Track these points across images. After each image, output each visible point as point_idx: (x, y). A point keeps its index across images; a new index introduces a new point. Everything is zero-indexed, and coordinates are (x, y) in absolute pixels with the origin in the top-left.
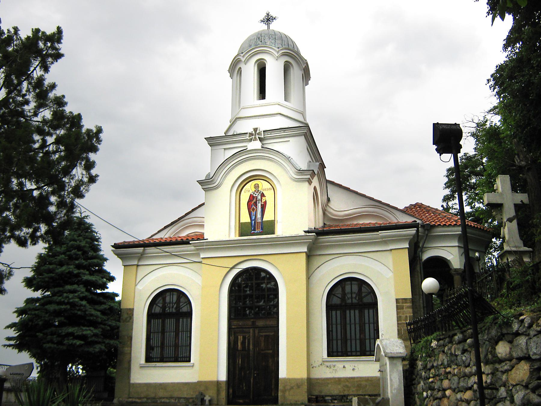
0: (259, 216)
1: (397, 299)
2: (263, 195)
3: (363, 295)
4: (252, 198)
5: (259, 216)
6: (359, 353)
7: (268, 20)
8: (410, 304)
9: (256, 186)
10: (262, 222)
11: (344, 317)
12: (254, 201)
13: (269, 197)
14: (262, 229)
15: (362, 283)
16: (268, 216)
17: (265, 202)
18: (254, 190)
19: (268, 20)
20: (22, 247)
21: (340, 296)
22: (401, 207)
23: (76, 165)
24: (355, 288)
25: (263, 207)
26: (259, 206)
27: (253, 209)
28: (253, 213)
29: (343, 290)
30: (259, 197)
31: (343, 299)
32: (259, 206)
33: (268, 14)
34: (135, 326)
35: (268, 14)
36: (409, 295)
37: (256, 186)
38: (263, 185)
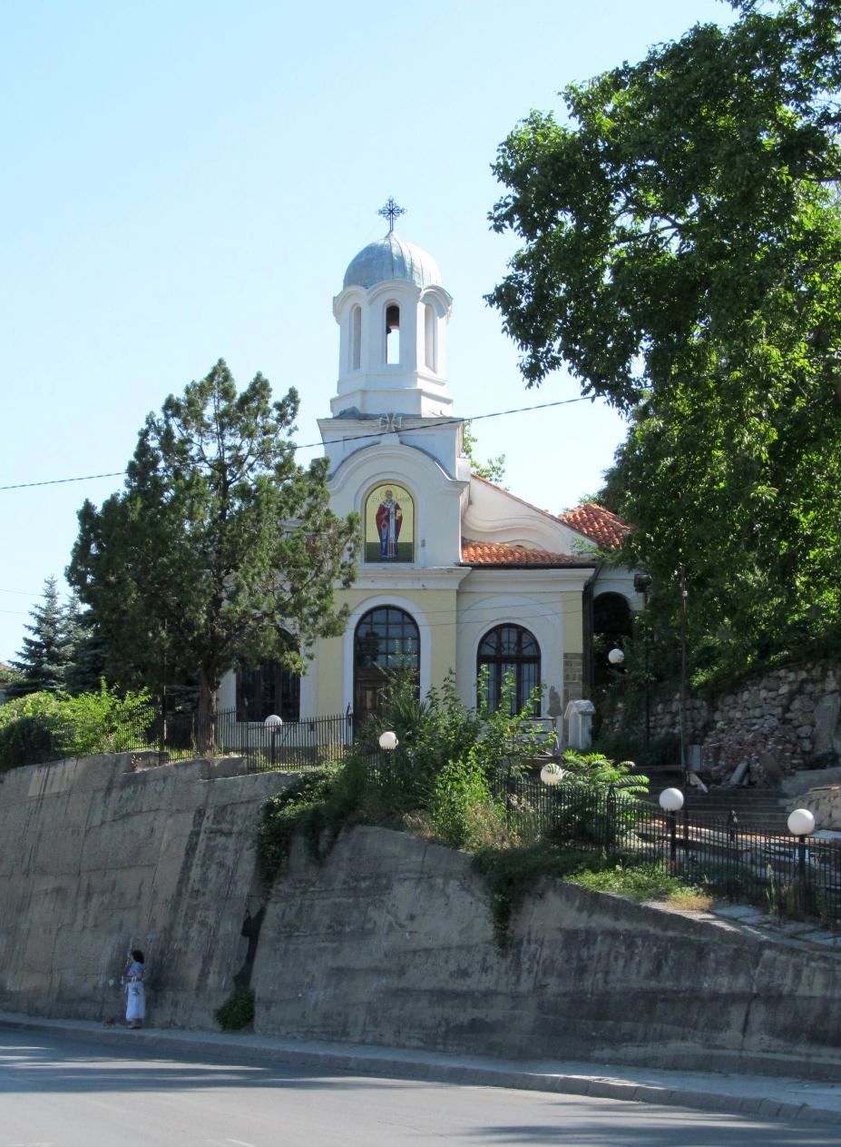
0: (392, 535)
1: (566, 656)
2: (397, 507)
3: (524, 646)
4: (382, 510)
5: (392, 535)
6: (410, 630)
7: (391, 212)
8: (580, 661)
9: (389, 494)
10: (396, 544)
11: (498, 673)
12: (386, 514)
13: (406, 510)
14: (396, 553)
15: (521, 631)
16: (405, 537)
17: (401, 518)
18: (385, 498)
19: (391, 212)
20: (345, 281)
21: (494, 645)
22: (557, 513)
23: (692, 885)
24: (514, 636)
25: (398, 523)
26: (392, 521)
27: (384, 526)
28: (384, 531)
29: (499, 637)
30: (392, 510)
31: (499, 648)
32: (392, 521)
33: (381, 212)
34: (436, 1087)
35: (381, 212)
36: (580, 650)
37: (389, 494)
38: (399, 494)
